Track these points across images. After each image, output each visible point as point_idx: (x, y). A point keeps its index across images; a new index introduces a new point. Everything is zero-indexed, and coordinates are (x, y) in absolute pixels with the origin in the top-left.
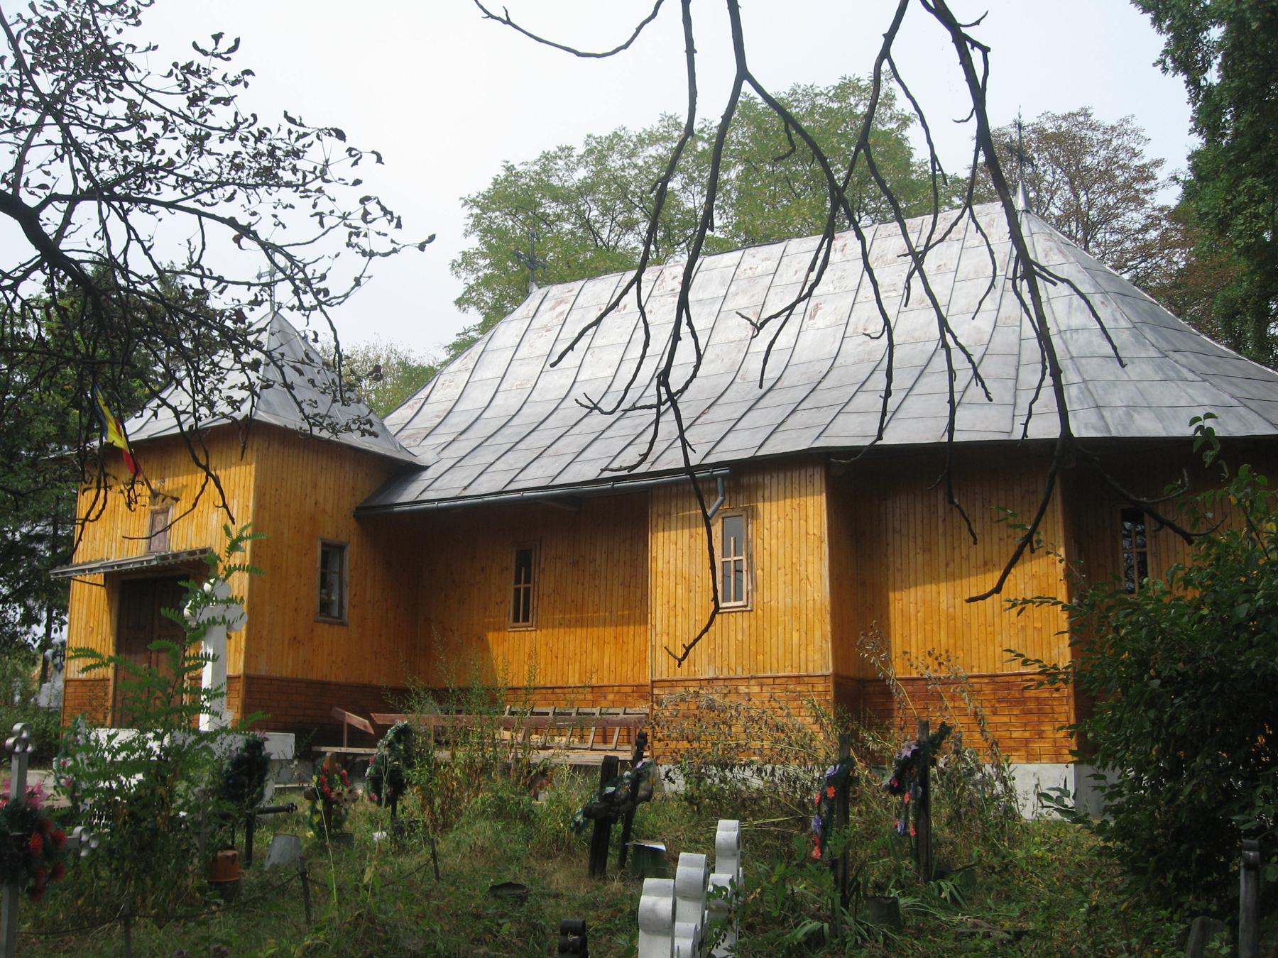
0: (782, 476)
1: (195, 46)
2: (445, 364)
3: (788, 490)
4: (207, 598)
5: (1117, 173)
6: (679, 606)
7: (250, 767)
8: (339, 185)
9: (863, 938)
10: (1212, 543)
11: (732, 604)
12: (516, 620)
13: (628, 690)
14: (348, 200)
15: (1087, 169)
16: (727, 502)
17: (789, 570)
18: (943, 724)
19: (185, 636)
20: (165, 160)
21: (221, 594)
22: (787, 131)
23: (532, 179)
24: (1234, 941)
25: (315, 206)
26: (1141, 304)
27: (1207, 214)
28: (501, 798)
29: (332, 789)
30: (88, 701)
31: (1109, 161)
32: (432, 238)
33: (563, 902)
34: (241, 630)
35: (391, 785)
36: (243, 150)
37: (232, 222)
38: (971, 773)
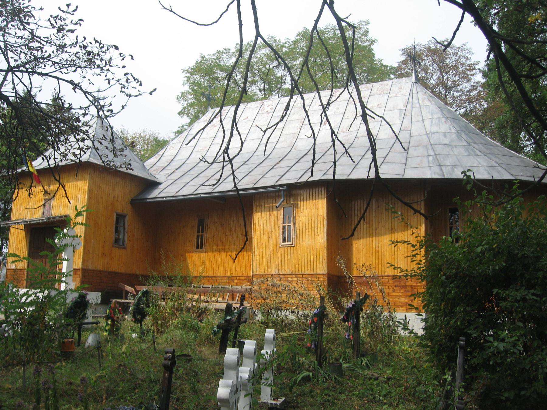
0: (308, 190)
1: (59, 8)
2: (173, 140)
3: (311, 196)
4: (65, 235)
5: (460, 67)
6: (264, 243)
7: (81, 304)
8: (116, 68)
9: (326, 379)
10: (471, 222)
11: (286, 243)
12: (197, 248)
13: (243, 278)
14: (119, 74)
15: (448, 65)
16: (285, 201)
17: (310, 230)
18: (366, 294)
19: (55, 252)
20: (47, 54)
21: (71, 233)
22: (276, 57)
23: (212, 61)
24: (453, 375)
25: (106, 76)
26: (462, 123)
27: (491, 84)
28: (185, 321)
29: (115, 315)
30: (15, 277)
31: (457, 61)
32: (155, 90)
33: (207, 363)
34: (80, 250)
35: (139, 315)
36: (80, 51)
37: (71, 82)
38: (380, 315)
